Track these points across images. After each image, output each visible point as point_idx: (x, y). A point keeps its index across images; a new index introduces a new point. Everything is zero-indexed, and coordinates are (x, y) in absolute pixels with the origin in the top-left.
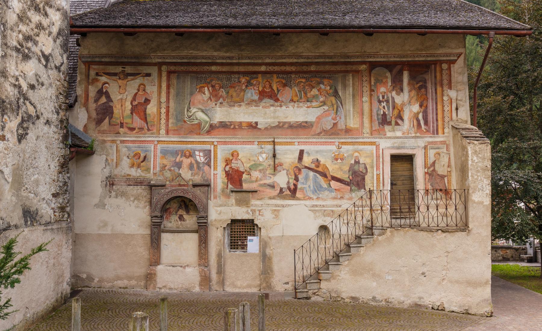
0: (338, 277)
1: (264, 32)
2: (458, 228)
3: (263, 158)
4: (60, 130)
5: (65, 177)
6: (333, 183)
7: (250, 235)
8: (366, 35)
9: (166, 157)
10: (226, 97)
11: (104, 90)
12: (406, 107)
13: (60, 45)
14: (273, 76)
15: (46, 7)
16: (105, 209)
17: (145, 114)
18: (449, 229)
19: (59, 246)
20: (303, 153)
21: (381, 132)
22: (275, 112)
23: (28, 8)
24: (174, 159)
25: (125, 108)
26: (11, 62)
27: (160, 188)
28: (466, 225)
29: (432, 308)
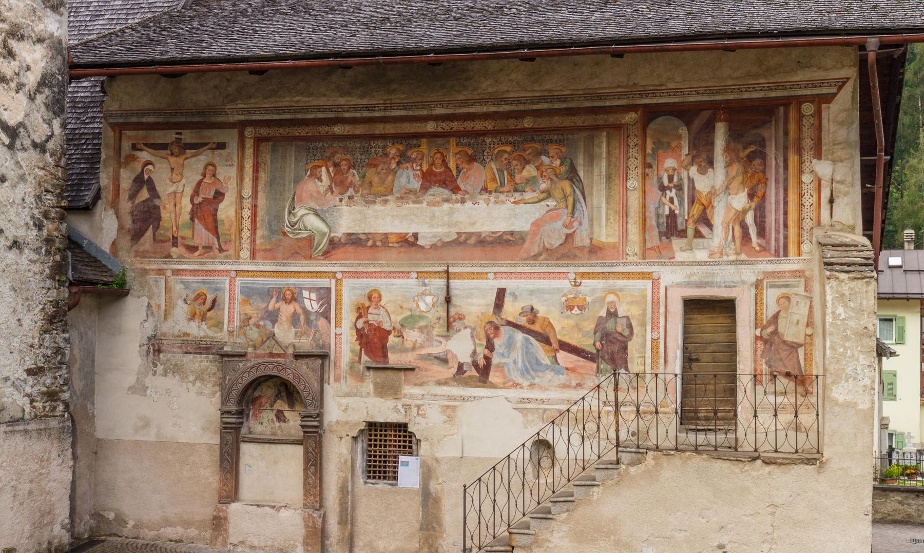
0: (547, 544)
3: (426, 304)
4: (46, 256)
5: (59, 339)
6: (562, 355)
7: (404, 453)
9: (251, 301)
10: (360, 186)
11: (146, 177)
12: (718, 199)
13: (45, 104)
14: (448, 141)
17: (215, 220)
19: (42, 461)
20: (504, 295)
22: (451, 212)
24: (264, 305)
27: (236, 359)
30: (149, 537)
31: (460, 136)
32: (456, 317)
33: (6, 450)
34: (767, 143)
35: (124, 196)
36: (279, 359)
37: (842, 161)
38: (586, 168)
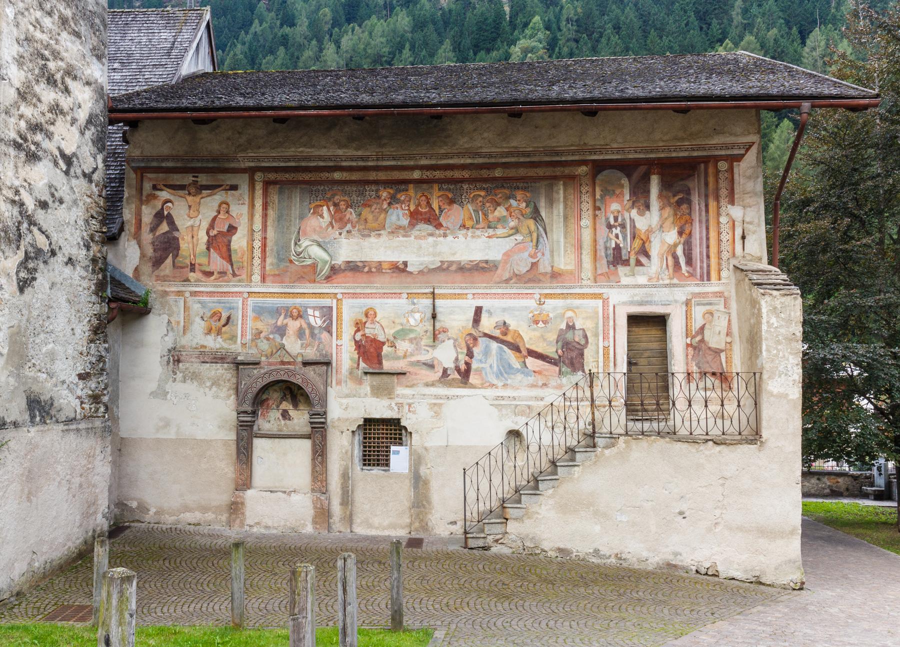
0: (536, 516)
1: (414, 114)
2: (744, 437)
3: (415, 320)
4: (92, 274)
5: (101, 349)
6: (530, 361)
7: (395, 444)
8: (586, 115)
9: (262, 318)
10: (357, 222)
11: (166, 213)
12: (654, 235)
13: (92, 140)
14: (432, 187)
15: (66, 79)
16: (166, 399)
17: (229, 250)
18: (727, 440)
19: (89, 457)
20: (481, 312)
21: (612, 278)
22: (435, 245)
23: (35, 79)
24: (274, 321)
25: (198, 240)
26: (6, 164)
27: (251, 366)
28: (757, 433)
29: (697, 572)
30: (170, 522)
31: (442, 183)
32: (441, 330)
33: (63, 447)
34: (692, 192)
35: (145, 229)
37: (750, 207)
38: (547, 210)
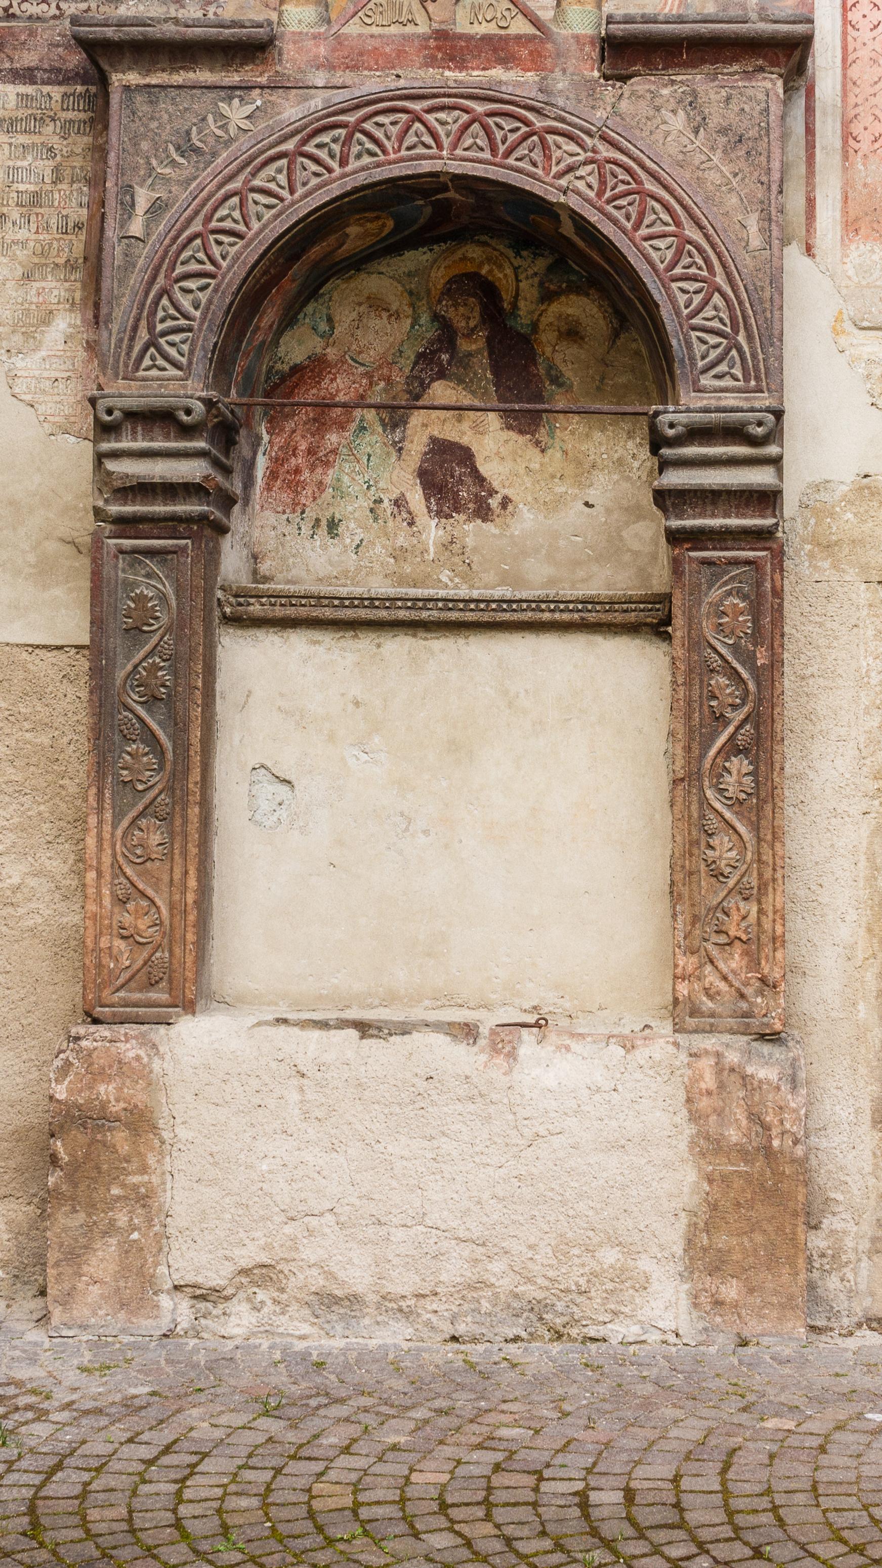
27: (204, 76)
36: (497, 73)
